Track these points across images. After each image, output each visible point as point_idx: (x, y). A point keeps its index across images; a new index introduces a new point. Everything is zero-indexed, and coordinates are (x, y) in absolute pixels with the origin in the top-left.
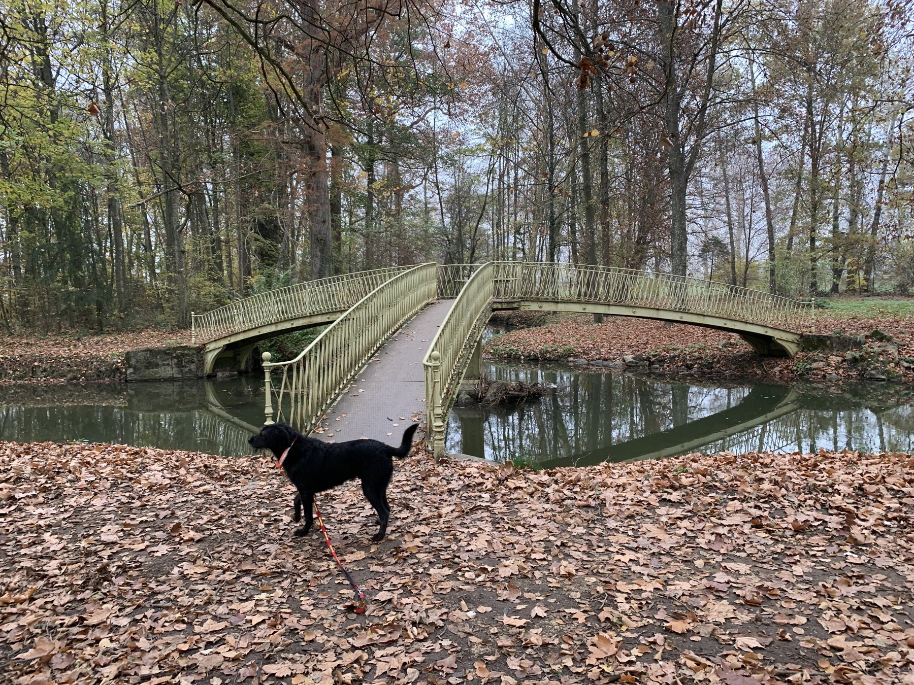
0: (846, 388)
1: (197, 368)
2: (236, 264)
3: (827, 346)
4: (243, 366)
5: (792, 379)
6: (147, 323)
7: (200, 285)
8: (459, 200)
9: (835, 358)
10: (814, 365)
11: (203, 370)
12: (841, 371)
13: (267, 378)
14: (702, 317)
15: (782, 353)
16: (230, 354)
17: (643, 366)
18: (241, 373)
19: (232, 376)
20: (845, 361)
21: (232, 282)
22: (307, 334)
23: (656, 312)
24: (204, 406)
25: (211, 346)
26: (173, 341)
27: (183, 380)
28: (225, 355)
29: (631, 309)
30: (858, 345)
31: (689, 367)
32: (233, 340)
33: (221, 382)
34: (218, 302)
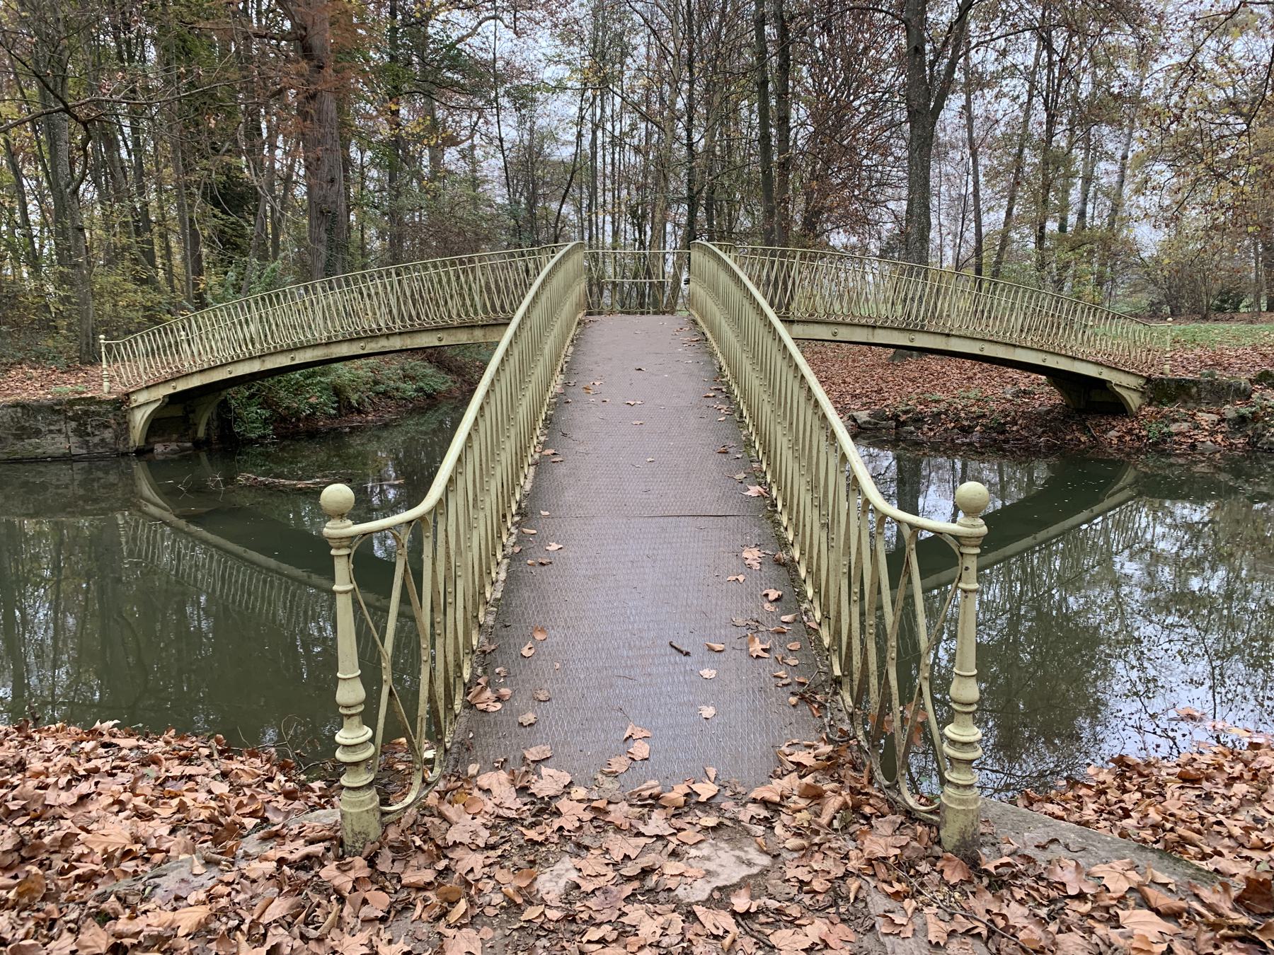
0: (1222, 464)
1: (117, 438)
2: (177, 259)
3: (1191, 397)
4: (201, 433)
5: (1139, 450)
6: (21, 355)
7: (116, 288)
8: (527, 167)
9: (1206, 416)
10: (1174, 428)
11: (126, 440)
12: (1219, 438)
13: (343, 582)
14: (1011, 349)
15: (1117, 407)
16: (177, 411)
17: (888, 429)
18: (198, 444)
19: (183, 450)
20: (1223, 420)
21: (172, 287)
22: (313, 375)
23: (944, 339)
24: (132, 501)
25: (142, 398)
26: (67, 387)
27: (90, 459)
28: (166, 414)
29: (907, 335)
30: (1245, 395)
31: (966, 431)
32: (182, 386)
33: (164, 461)
34: (150, 318)
